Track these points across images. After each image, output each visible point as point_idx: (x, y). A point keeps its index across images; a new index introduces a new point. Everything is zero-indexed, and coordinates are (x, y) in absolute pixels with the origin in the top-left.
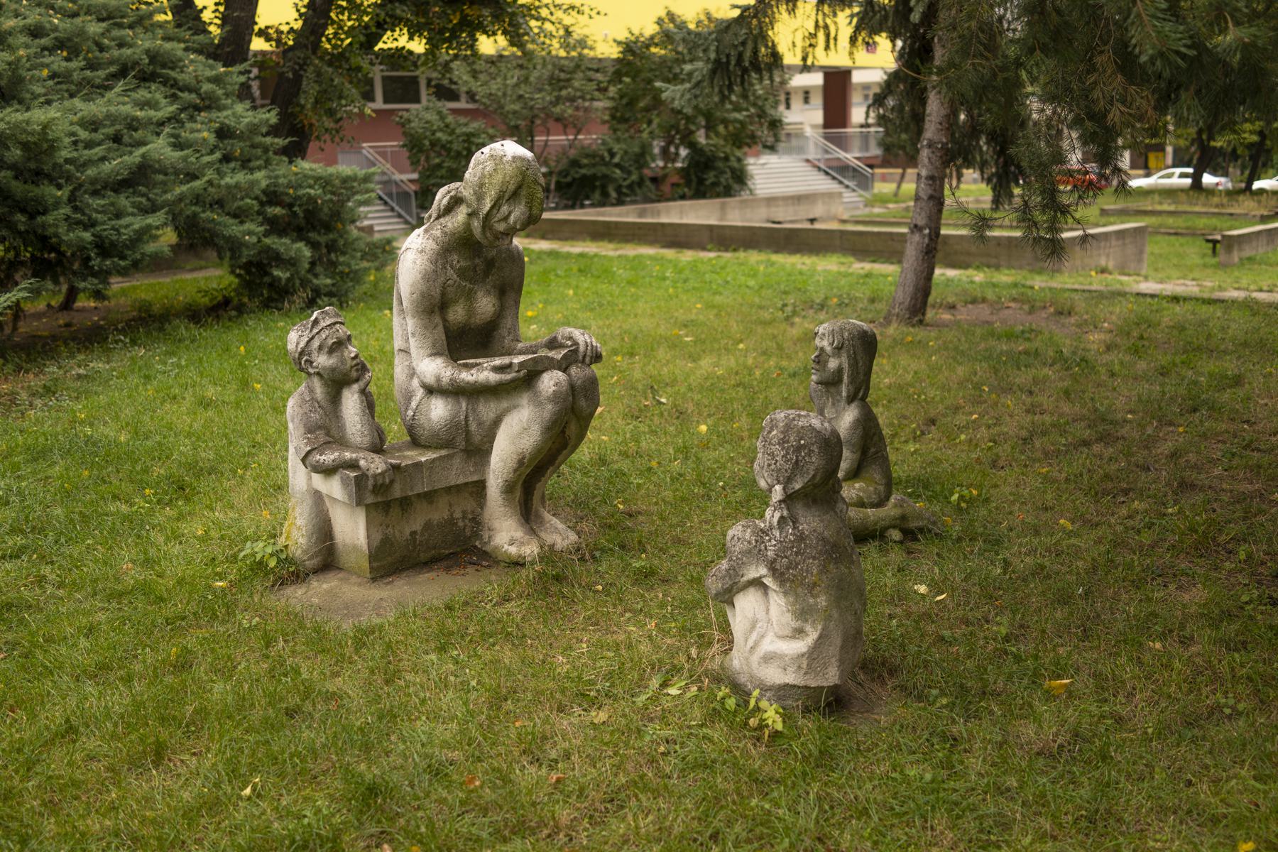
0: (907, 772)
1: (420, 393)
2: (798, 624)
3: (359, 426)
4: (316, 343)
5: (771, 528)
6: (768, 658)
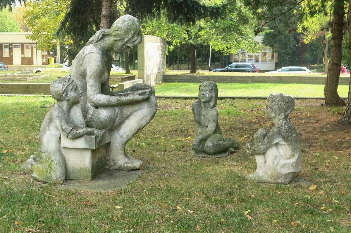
0: (315, 229)
1: (92, 109)
2: (292, 154)
3: (82, 120)
4: (70, 87)
5: (282, 126)
6: (283, 166)
